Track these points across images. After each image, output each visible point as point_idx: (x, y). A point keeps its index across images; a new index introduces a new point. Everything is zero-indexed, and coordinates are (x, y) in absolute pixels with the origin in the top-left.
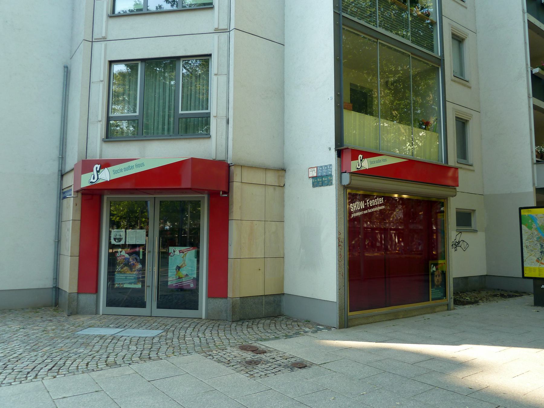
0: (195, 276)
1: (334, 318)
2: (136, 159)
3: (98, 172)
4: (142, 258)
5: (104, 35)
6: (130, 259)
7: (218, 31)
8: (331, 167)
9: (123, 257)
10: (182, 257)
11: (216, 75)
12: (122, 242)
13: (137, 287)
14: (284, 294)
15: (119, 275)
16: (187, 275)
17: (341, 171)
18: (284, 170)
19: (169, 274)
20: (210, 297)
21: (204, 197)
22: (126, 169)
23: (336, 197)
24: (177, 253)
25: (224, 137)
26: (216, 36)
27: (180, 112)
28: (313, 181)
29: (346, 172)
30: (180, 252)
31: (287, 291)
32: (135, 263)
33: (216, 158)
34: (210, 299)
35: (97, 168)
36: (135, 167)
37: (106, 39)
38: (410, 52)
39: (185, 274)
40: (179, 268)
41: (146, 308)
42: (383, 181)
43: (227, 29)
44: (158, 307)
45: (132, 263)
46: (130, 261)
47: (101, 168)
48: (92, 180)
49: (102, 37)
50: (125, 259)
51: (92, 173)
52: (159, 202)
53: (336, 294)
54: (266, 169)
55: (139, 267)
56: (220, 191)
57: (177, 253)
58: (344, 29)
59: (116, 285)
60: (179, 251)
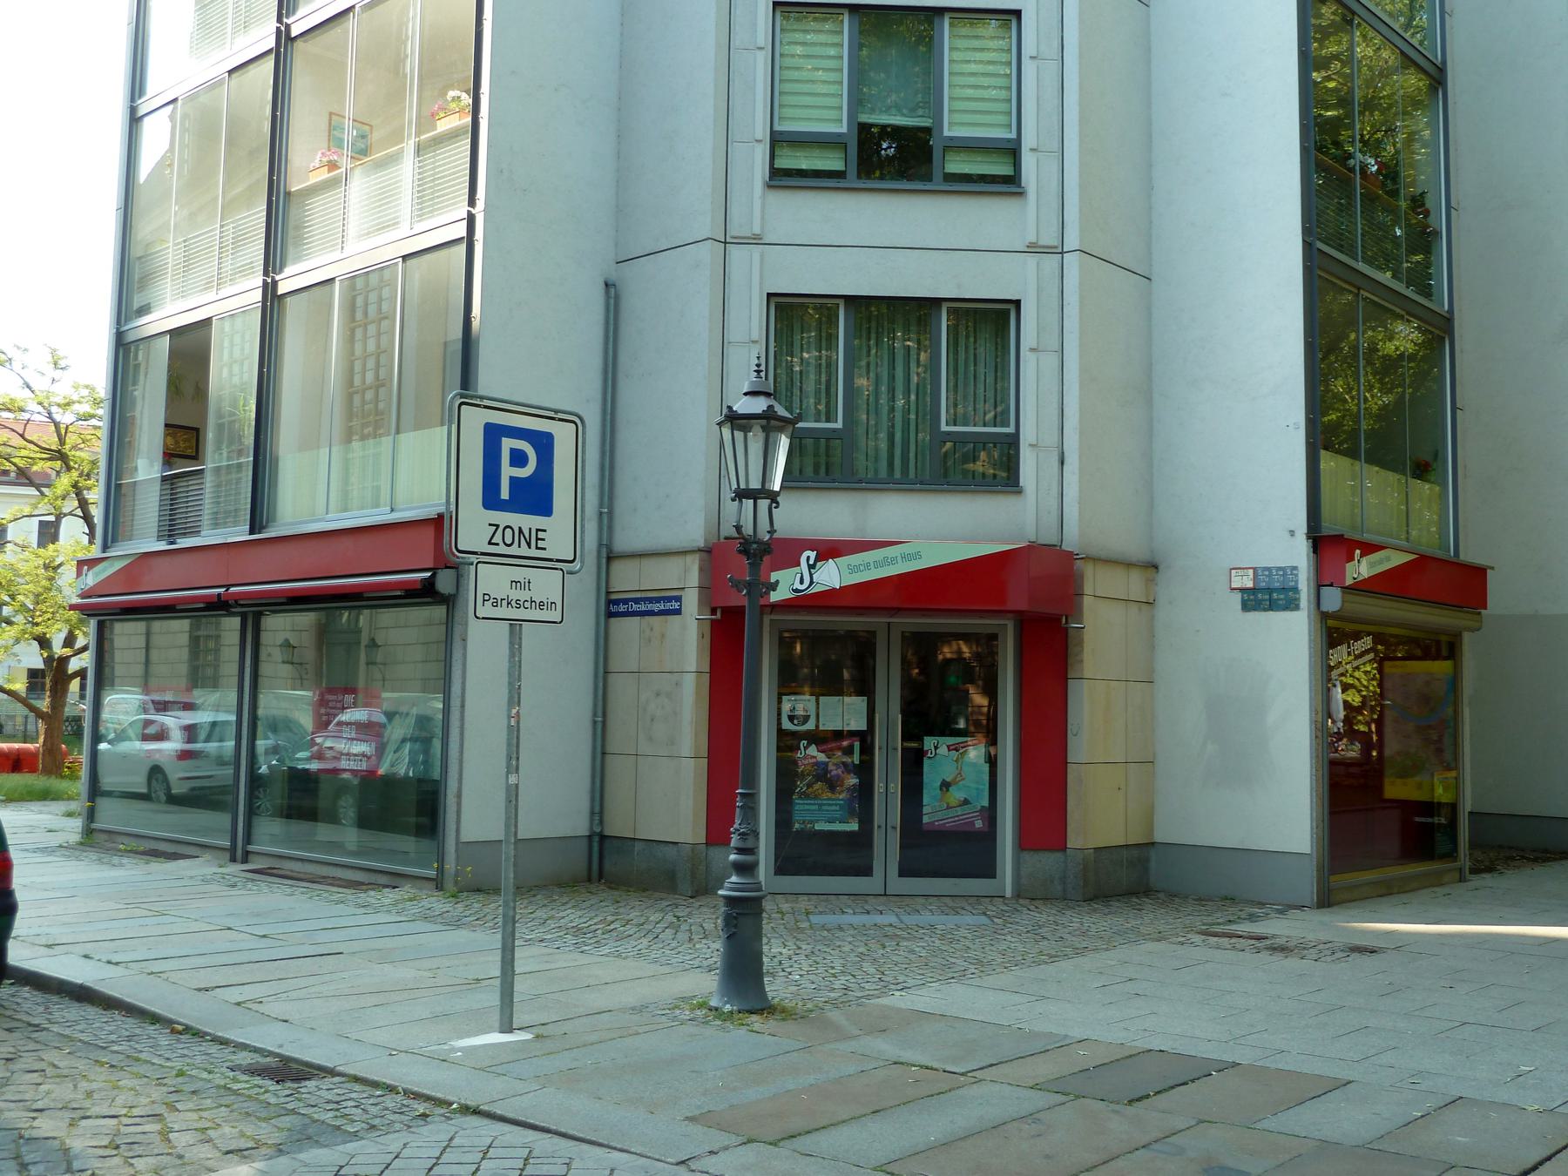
0: (986, 803)
1: (1307, 885)
2: (901, 543)
3: (811, 567)
4: (858, 763)
5: (757, 230)
6: (830, 764)
7: (1034, 249)
8: (1295, 572)
9: (811, 761)
10: (955, 759)
11: (1032, 350)
12: (810, 726)
13: (849, 830)
14: (1153, 844)
15: (801, 802)
16: (966, 802)
17: (1320, 582)
18: (1156, 567)
19: (926, 800)
20: (1025, 850)
21: (1006, 625)
22: (878, 565)
23: (1310, 635)
24: (943, 750)
25: (1055, 490)
26: (1032, 260)
27: (944, 428)
28: (1243, 597)
29: (1331, 585)
30: (949, 750)
31: (1164, 833)
32: (840, 773)
33: (1037, 538)
34: (1025, 852)
35: (808, 558)
36: (899, 559)
37: (761, 239)
38: (1404, 310)
39: (962, 799)
40: (945, 785)
41: (872, 876)
42: (1361, 598)
43: (1056, 247)
44: (903, 873)
45: (834, 773)
46: (829, 769)
47: (818, 559)
48: (797, 586)
49: (754, 235)
50: (817, 764)
51: (797, 569)
52: (873, 629)
53: (1309, 837)
54: (1129, 565)
55: (851, 784)
56: (1062, 616)
57: (943, 750)
58: (1320, 276)
59: (797, 826)
60: (948, 747)
